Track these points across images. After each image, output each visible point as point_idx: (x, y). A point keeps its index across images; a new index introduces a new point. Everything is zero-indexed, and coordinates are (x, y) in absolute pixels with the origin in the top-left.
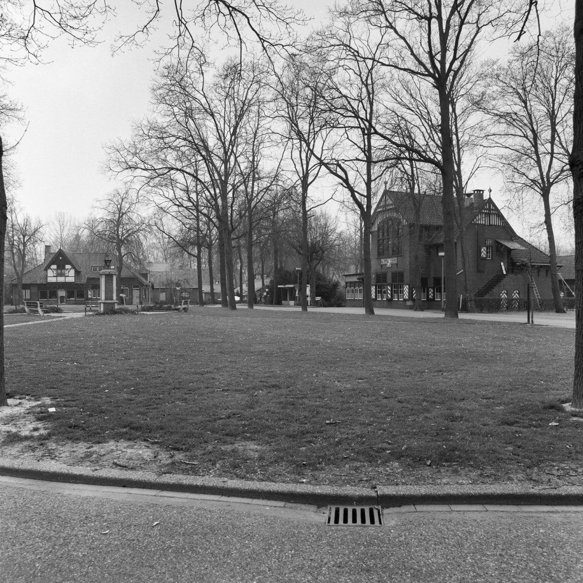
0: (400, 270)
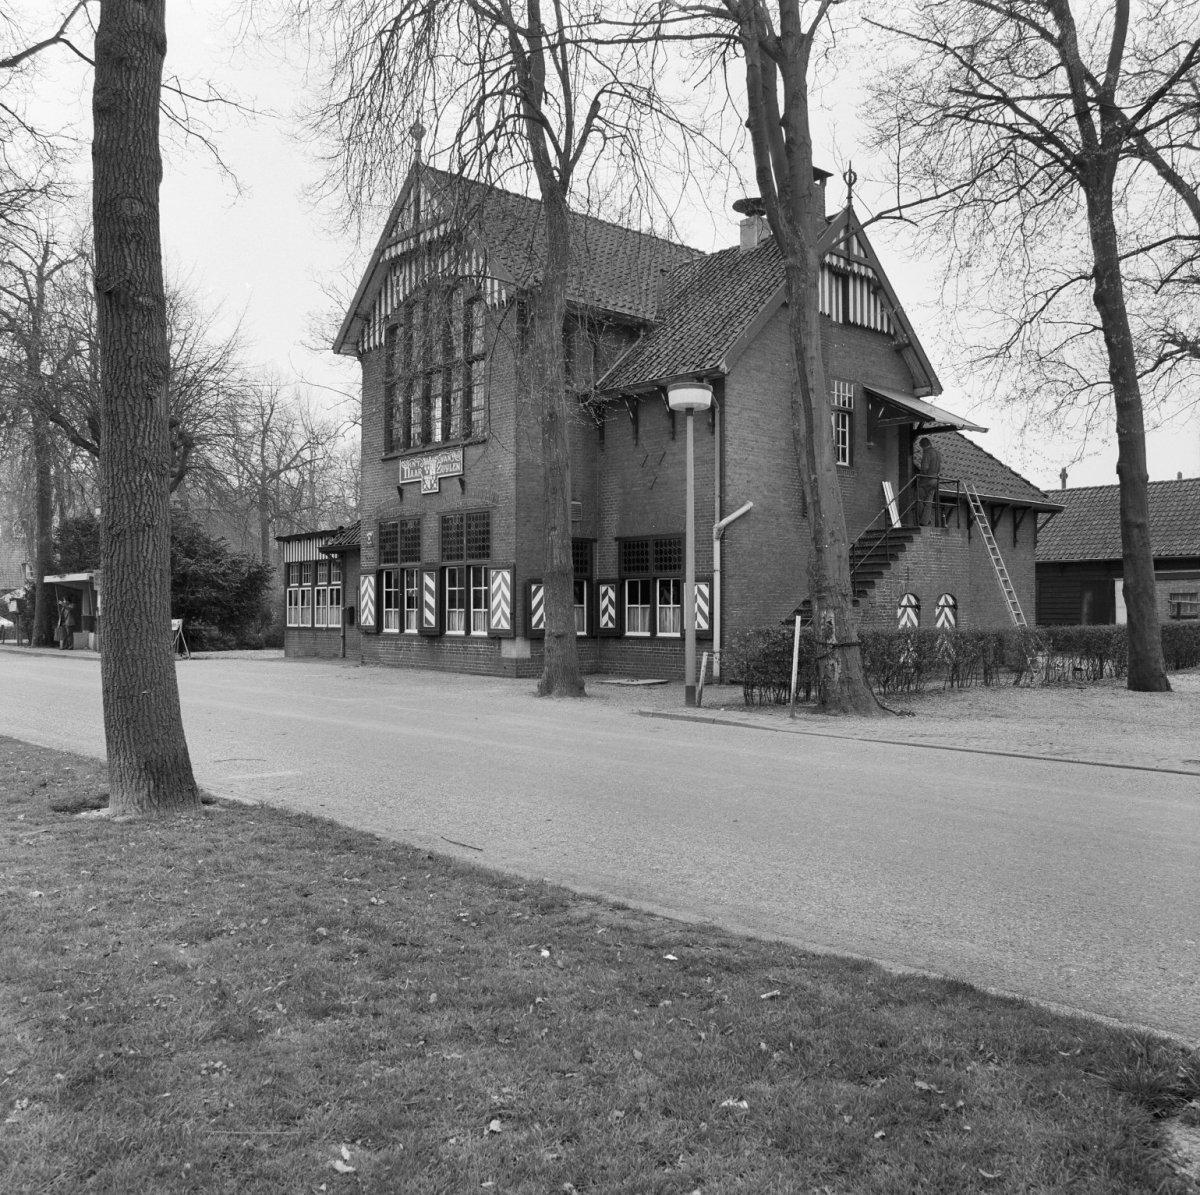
0: (473, 502)
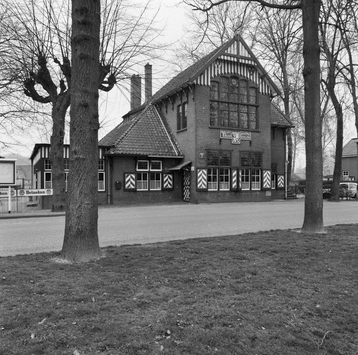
0: (254, 149)
